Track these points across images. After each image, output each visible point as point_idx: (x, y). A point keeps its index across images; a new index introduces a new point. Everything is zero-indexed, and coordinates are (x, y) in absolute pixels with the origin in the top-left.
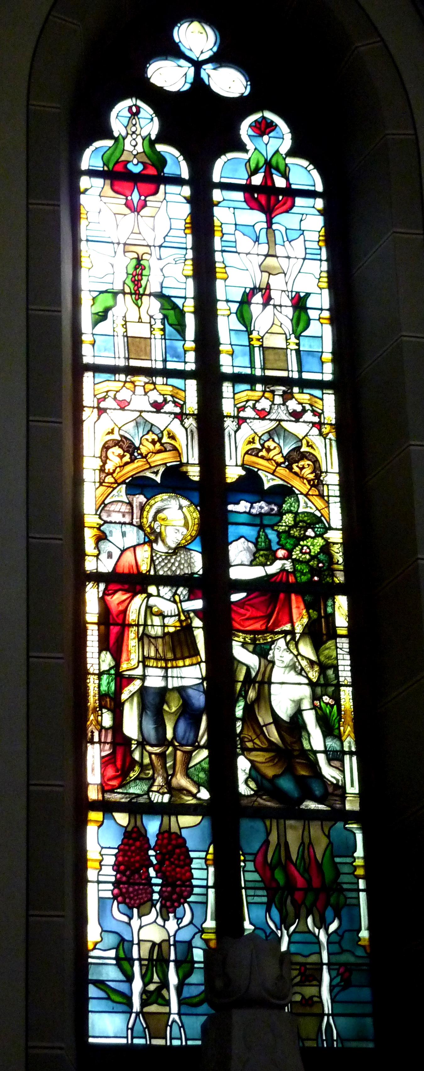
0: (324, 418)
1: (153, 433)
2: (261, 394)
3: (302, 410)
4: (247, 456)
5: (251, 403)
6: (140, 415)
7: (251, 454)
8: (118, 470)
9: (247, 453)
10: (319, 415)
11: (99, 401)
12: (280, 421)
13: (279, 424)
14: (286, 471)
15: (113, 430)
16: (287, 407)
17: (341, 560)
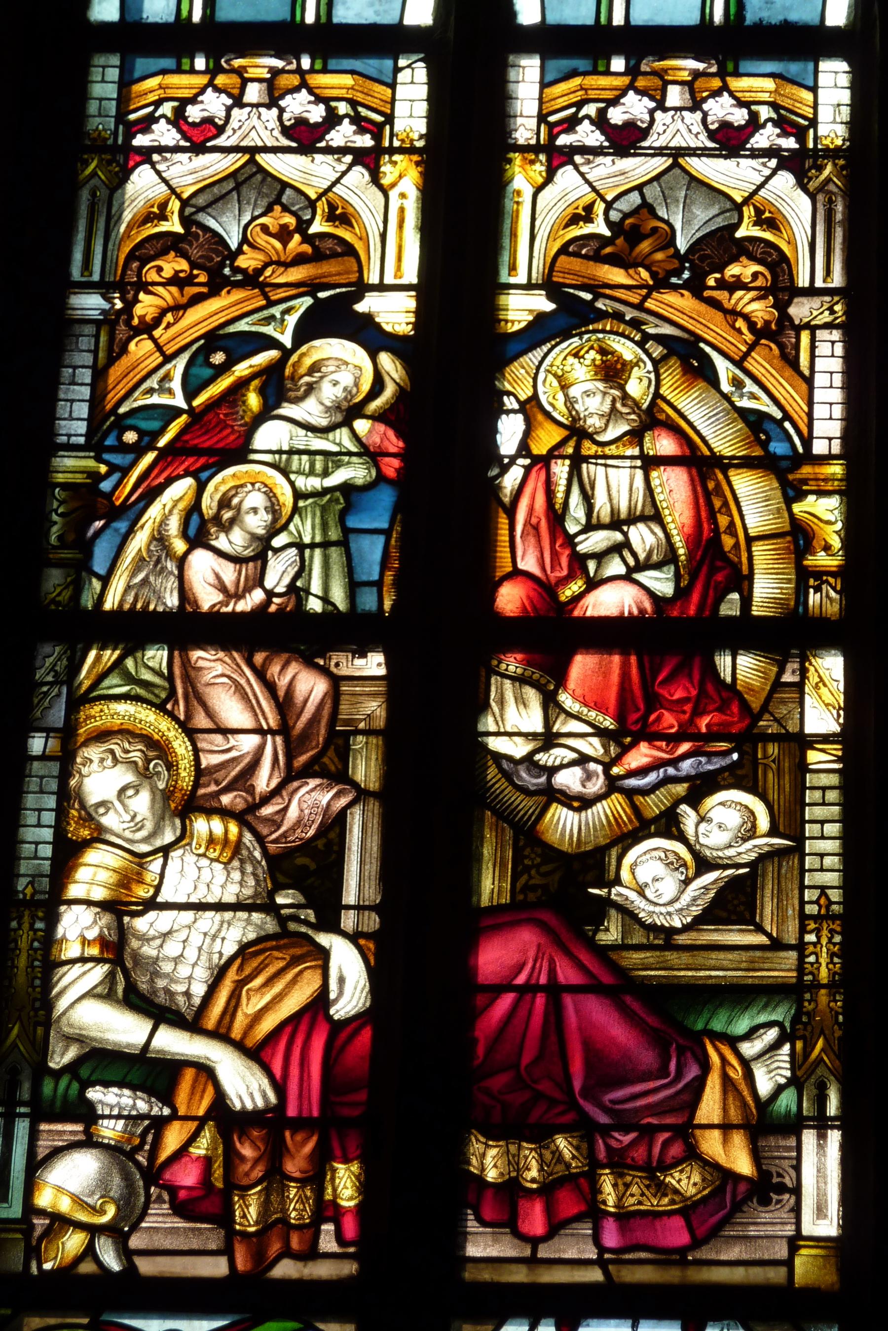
0: (392, 135)
1: (286, 209)
2: (203, 80)
3: (748, 122)
4: (562, 258)
5: (591, 109)
7: (570, 254)
8: (169, 317)
9: (564, 250)
10: (800, 134)
11: (554, 131)
12: (253, 151)
13: (252, 161)
14: (682, 295)
16: (705, 115)
17: (836, 543)
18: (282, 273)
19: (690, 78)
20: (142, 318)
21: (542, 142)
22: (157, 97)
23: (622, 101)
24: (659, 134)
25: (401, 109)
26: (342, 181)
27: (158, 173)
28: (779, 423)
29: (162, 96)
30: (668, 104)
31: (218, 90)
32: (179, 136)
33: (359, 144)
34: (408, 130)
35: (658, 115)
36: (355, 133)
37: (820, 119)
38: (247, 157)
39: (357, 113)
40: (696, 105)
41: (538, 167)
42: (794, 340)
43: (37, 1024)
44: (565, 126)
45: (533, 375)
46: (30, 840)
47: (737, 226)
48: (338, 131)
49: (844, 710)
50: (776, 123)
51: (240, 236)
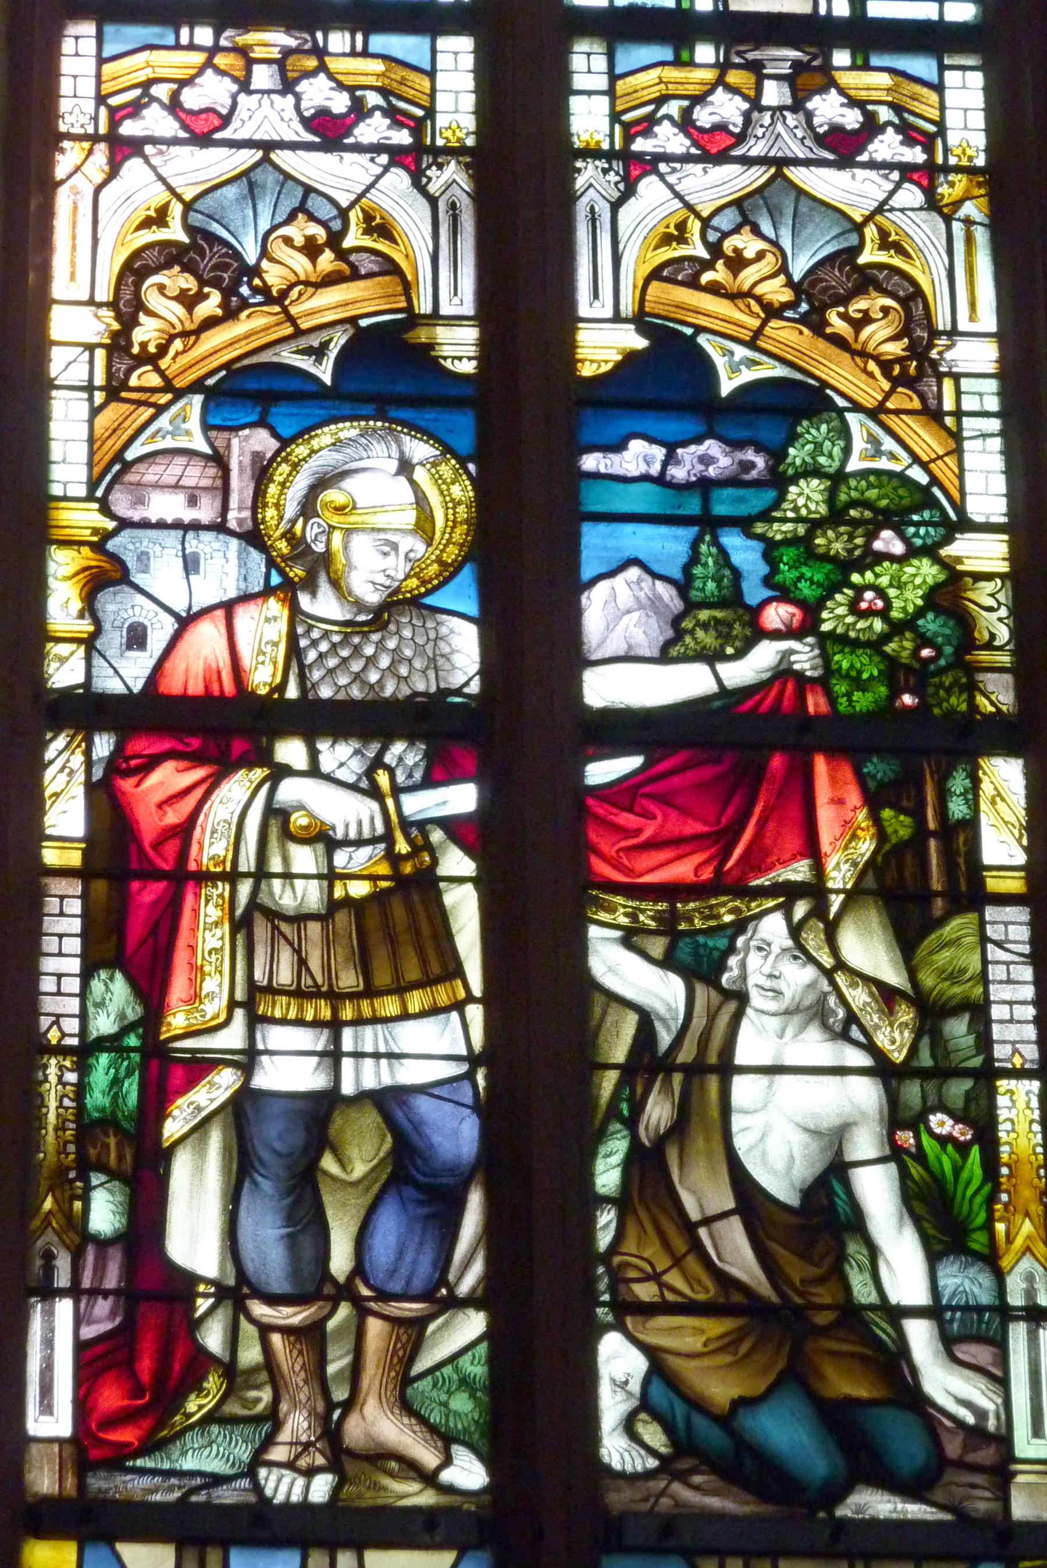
1: (312, 218)
5: (673, 108)
6: (266, 160)
8: (178, 344)
9: (656, 274)
10: (928, 143)
11: (116, 116)
15: (681, 226)
17: (1003, 634)
18: (314, 294)
19: (280, 56)
20: (144, 345)
21: (617, 147)
22: (658, 94)
23: (709, 99)
24: (243, 122)
25: (443, 102)
26: (377, 186)
27: (670, 187)
28: (926, 490)
29: (663, 92)
30: (765, 101)
31: (221, 72)
32: (688, 142)
33: (395, 141)
34: (964, 144)
35: (242, 98)
36: (389, 128)
37: (439, 107)
38: (773, 170)
39: (389, 103)
40: (288, 86)
41: (612, 177)
42: (935, 389)
43: (74, 1197)
44: (130, 109)
45: (134, 406)
46: (51, 971)
47: (858, 249)
48: (882, 142)
49: (1025, 829)
50: (898, 129)
51: (259, 249)
